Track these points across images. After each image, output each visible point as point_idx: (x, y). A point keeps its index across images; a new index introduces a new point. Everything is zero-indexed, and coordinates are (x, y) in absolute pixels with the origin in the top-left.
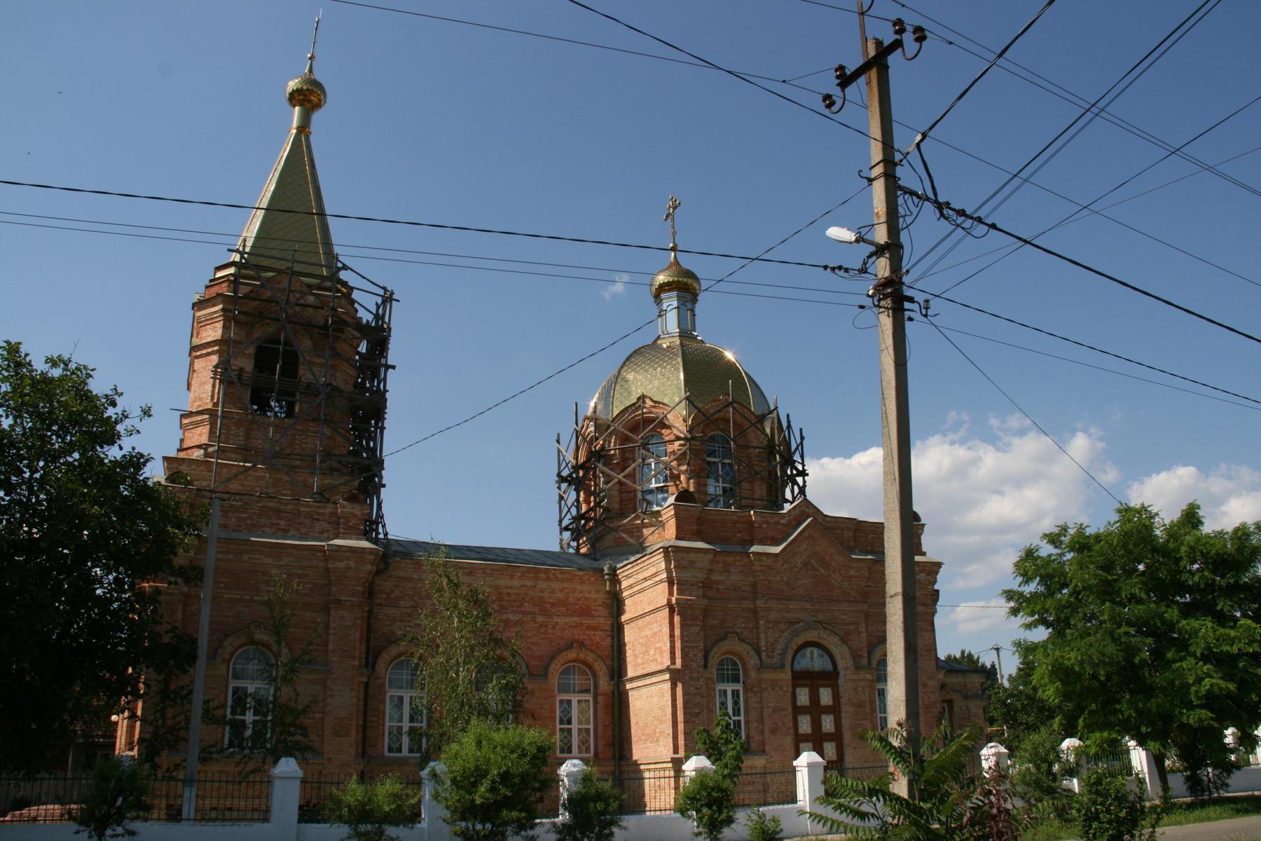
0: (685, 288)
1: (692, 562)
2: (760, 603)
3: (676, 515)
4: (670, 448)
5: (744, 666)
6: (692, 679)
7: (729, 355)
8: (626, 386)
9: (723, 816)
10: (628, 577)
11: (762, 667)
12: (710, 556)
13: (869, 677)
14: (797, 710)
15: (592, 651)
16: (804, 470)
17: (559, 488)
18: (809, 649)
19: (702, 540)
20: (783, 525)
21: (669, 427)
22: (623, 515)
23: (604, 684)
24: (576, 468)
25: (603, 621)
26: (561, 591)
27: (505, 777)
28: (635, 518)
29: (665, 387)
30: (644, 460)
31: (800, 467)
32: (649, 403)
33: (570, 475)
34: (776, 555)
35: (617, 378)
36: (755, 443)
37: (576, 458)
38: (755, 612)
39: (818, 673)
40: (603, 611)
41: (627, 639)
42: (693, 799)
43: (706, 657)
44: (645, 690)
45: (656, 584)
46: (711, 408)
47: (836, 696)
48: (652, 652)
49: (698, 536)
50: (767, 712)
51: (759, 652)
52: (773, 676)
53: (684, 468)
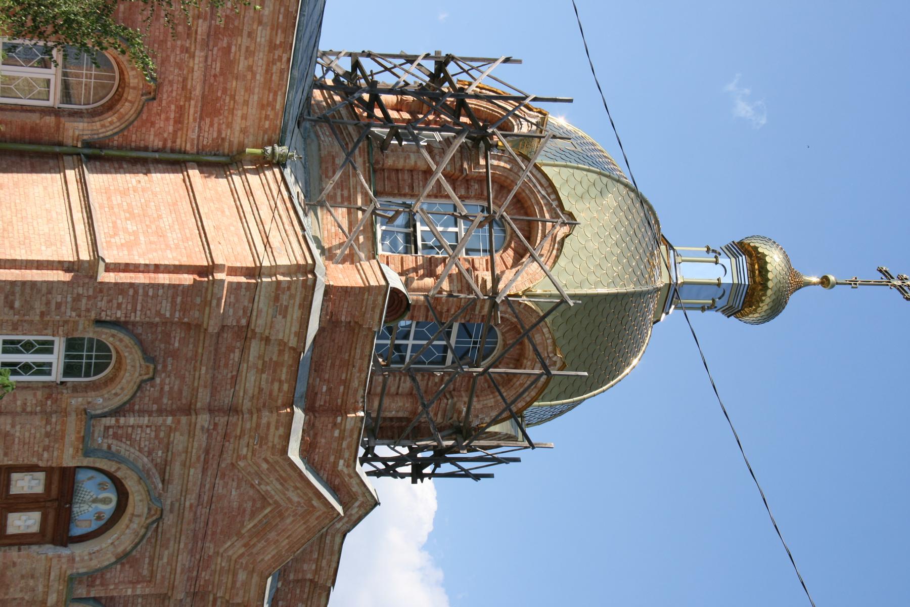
0: (754, 297)
1: (284, 312)
2: (204, 420)
4: (480, 260)
5: (94, 386)
6: (77, 299)
7: (635, 362)
8: (594, 192)
10: (266, 186)
11: (89, 417)
12: (293, 342)
15: (139, 113)
16: (422, 477)
17: (427, 56)
18: (114, 497)
19: (321, 330)
20: (335, 464)
21: (517, 261)
22: (375, 171)
23: (77, 130)
24: (460, 94)
25: (191, 137)
26: (250, 68)
28: (365, 194)
29: (583, 262)
30: (465, 217)
31: (428, 470)
32: (561, 231)
33: (447, 78)
34: (284, 450)
35: (608, 175)
37: (476, 96)
38: (189, 410)
39: (70, 510)
40: (209, 137)
41: (156, 177)
44: (62, 207)
45: (251, 244)
46: (543, 337)
47: (23, 540)
48: (131, 226)
49: (329, 324)
51: (117, 412)
52: (71, 436)
53: (446, 285)
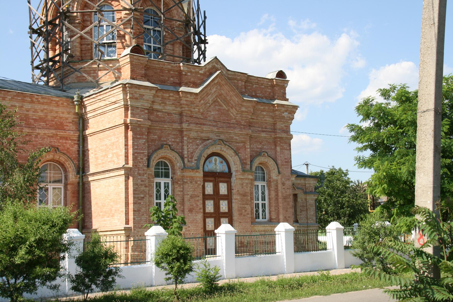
1: (142, 96)
2: (185, 126)
3: (131, 62)
4: (117, 16)
5: (173, 166)
6: (139, 174)
9: (187, 267)
10: (91, 104)
11: (184, 168)
12: (154, 92)
13: (250, 177)
14: (206, 197)
17: (31, 37)
18: (214, 158)
19: (148, 81)
20: (201, 74)
22: (82, 60)
23: (73, 177)
24: (46, 23)
25: (73, 134)
26: (42, 111)
27: (40, 242)
28: (92, 64)
34: (196, 94)
36: (176, 18)
38: (181, 131)
41: (90, 147)
42: (167, 255)
43: (149, 160)
45: (115, 109)
47: (230, 189)
48: (110, 156)
49: (146, 77)
50: (187, 198)
51: (182, 158)
52: (191, 174)
53: (128, 30)
